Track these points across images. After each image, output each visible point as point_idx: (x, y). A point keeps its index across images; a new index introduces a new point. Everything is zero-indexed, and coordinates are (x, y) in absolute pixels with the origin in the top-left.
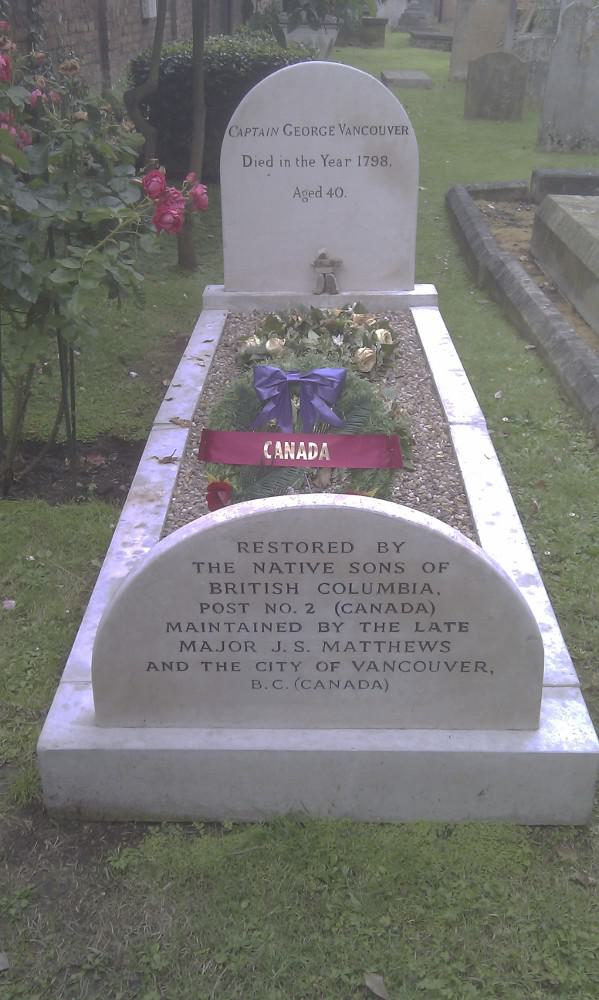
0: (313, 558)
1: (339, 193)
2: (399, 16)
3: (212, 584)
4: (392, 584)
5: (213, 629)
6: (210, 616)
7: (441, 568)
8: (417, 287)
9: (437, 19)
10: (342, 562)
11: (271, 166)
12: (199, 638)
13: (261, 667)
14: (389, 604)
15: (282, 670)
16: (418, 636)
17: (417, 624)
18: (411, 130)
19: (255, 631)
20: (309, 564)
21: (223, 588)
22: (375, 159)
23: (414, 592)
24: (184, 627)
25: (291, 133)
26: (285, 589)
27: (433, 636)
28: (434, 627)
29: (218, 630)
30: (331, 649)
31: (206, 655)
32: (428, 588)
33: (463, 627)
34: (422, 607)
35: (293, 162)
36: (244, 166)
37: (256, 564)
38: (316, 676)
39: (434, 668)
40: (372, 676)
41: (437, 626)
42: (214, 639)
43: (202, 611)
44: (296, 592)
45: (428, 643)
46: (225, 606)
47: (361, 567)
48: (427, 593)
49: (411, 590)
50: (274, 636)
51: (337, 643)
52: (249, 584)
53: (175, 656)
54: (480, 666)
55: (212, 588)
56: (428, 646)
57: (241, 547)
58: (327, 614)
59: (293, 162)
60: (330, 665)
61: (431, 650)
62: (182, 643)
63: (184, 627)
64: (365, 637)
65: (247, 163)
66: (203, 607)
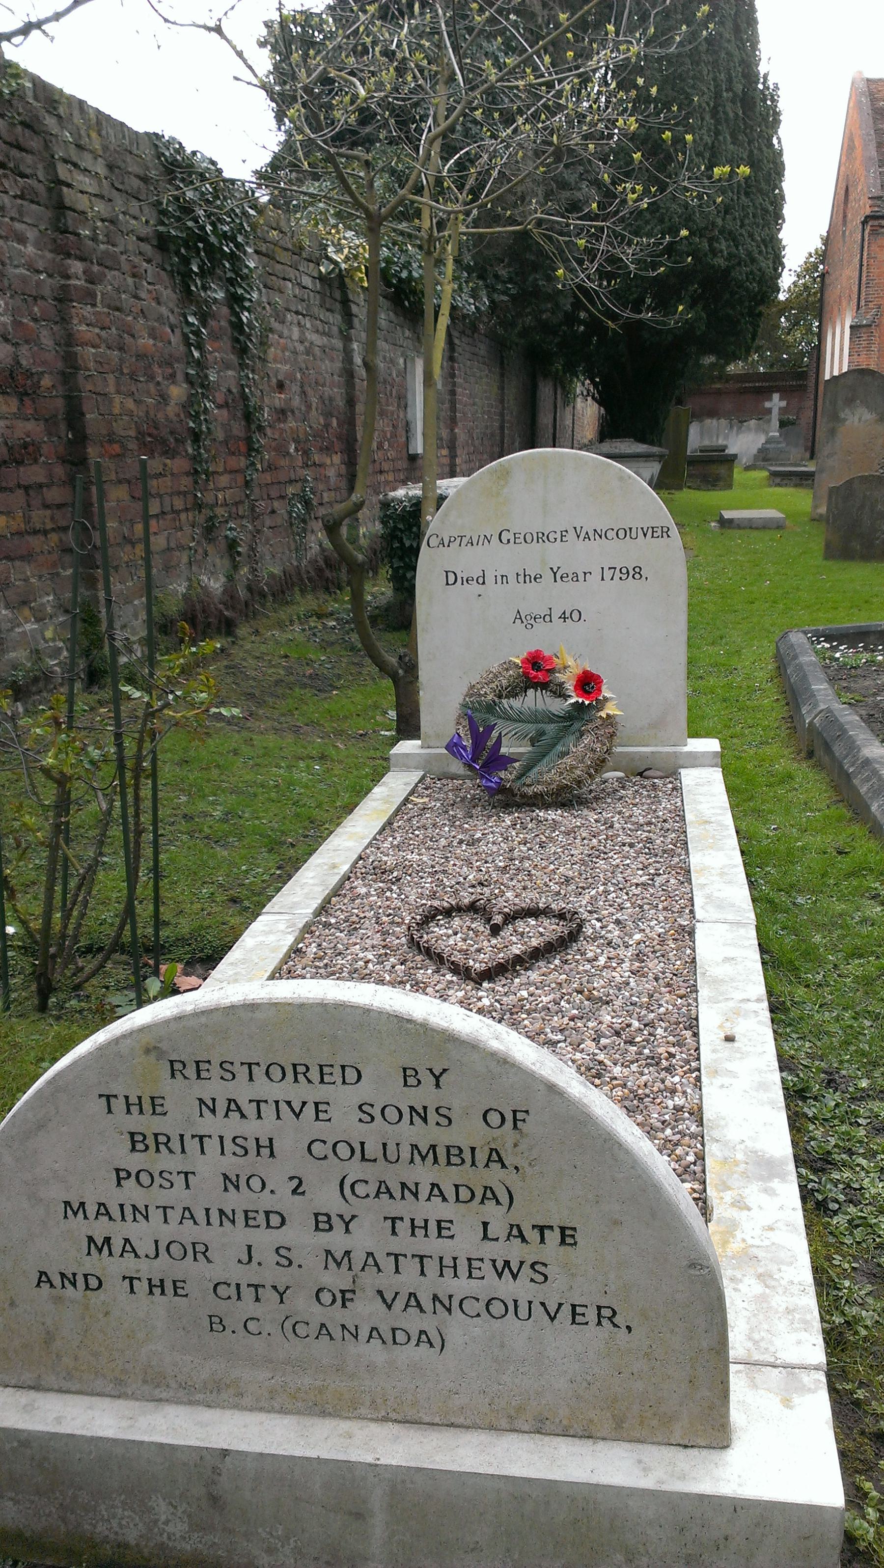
0: (297, 1092)
1: (575, 616)
2: (755, 451)
3: (132, 1135)
4: (433, 1147)
6: (131, 1192)
7: (515, 1120)
8: (690, 741)
9: (808, 455)
10: (343, 1099)
11: (484, 583)
12: (118, 1231)
13: (221, 1289)
15: (257, 1299)
16: (489, 1250)
17: (485, 1225)
18: (674, 531)
19: (209, 1223)
20: (289, 1103)
21: (150, 1141)
23: (473, 1164)
24: (91, 1209)
25: (509, 541)
26: (253, 1151)
27: (515, 1251)
28: (515, 1232)
29: (146, 1218)
30: (339, 1264)
31: (129, 1264)
32: (496, 1157)
33: (567, 1235)
34: (489, 1194)
35: (512, 578)
36: (447, 584)
37: (201, 1100)
38: (316, 1313)
39: (523, 1312)
40: (413, 1322)
41: (520, 1231)
42: (142, 1233)
43: (119, 1184)
44: (272, 1154)
45: (507, 1263)
48: (496, 1166)
49: (468, 1160)
50: (240, 1235)
51: (347, 1253)
52: (193, 1136)
55: (133, 1143)
56: (505, 1268)
59: (512, 578)
60: (339, 1296)
61: (515, 1276)
62: (91, 1239)
63: (91, 1209)
65: (451, 581)
66: (121, 1176)
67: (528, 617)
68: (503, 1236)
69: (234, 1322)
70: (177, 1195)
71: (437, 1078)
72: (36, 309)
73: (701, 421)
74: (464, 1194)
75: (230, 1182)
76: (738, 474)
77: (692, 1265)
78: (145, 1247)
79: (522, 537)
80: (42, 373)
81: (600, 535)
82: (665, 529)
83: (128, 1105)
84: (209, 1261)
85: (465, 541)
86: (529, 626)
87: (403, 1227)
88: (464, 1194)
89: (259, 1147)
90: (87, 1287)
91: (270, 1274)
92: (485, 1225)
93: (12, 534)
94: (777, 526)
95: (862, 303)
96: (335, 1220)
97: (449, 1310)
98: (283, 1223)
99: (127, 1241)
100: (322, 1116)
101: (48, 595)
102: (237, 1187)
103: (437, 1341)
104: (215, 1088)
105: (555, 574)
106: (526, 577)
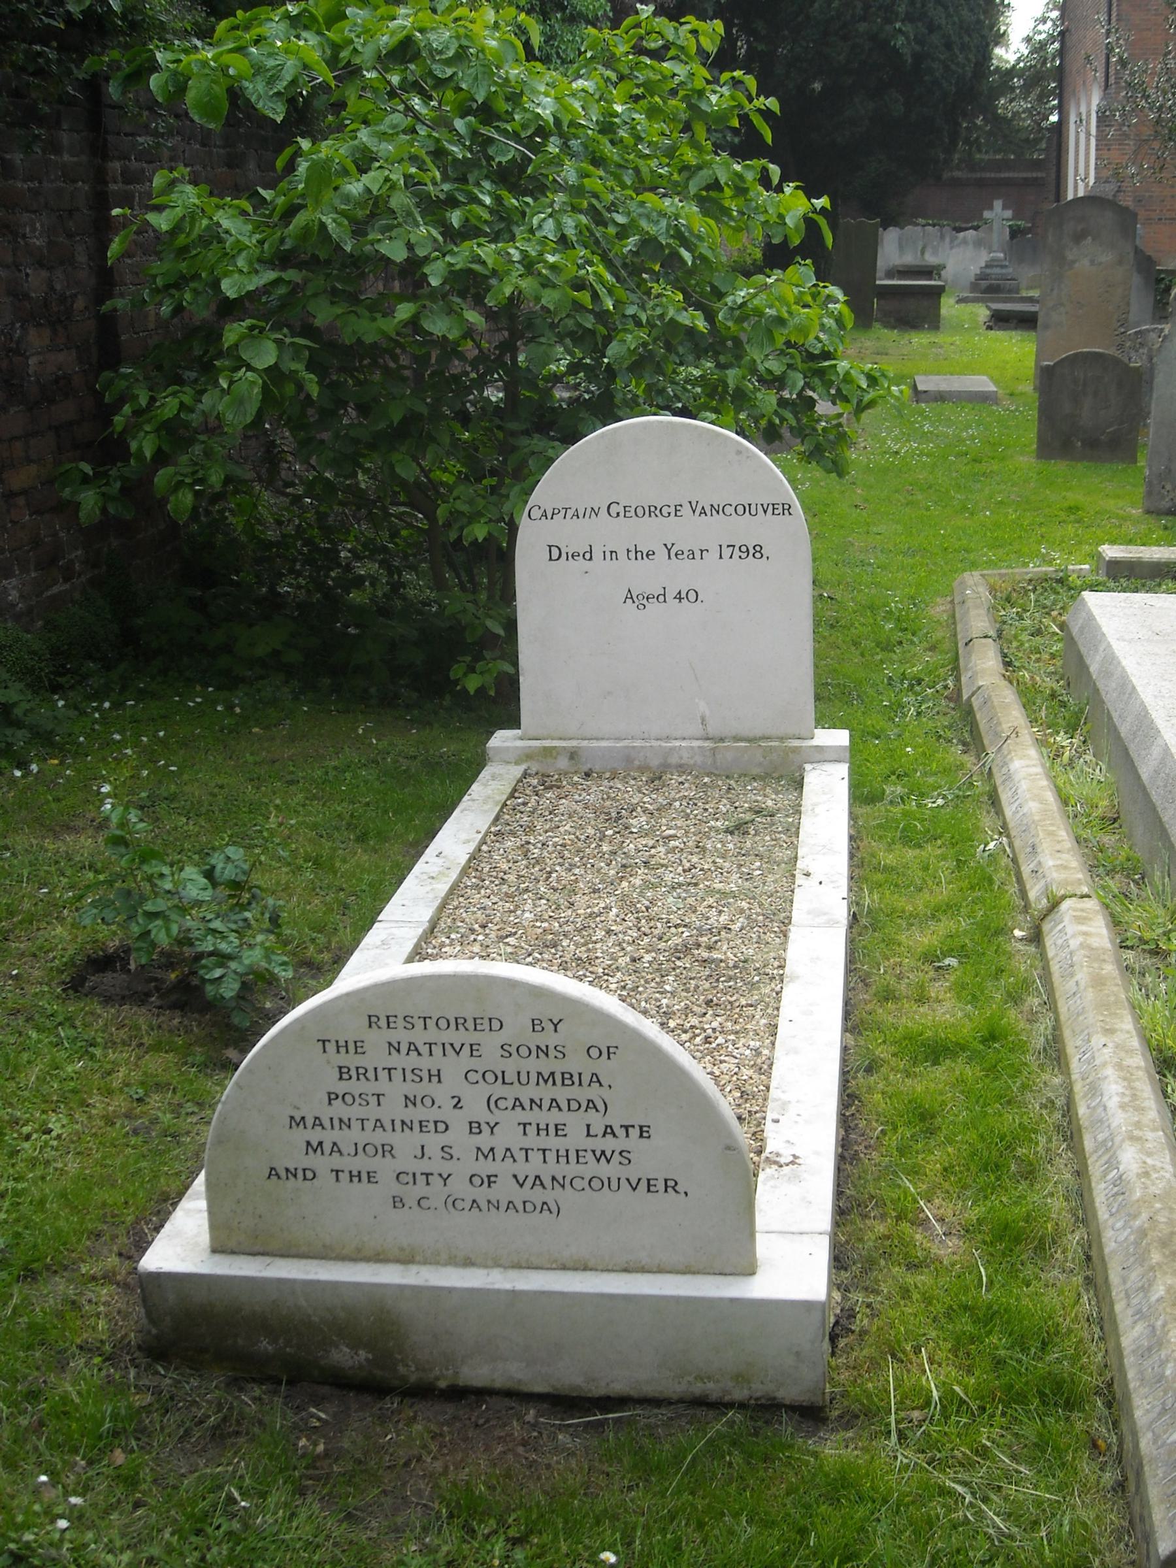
1: (692, 596)
3: (340, 1068)
4: (552, 1074)
5: (343, 1126)
8: (819, 732)
10: (491, 1042)
11: (591, 559)
14: (552, 1100)
15: (428, 1184)
16: (590, 1143)
20: (452, 1045)
21: (353, 1073)
22: (743, 549)
23: (580, 1084)
25: (618, 514)
26: (426, 1078)
27: (609, 1144)
30: (486, 1157)
31: (336, 1161)
32: (596, 1079)
33: (643, 1132)
35: (622, 555)
36: (551, 559)
38: (470, 1193)
40: (538, 1196)
42: (347, 1138)
43: (330, 1104)
44: (439, 1081)
45: (603, 1152)
46: (357, 1097)
47: (513, 1050)
49: (577, 1082)
51: (492, 1149)
53: (301, 1160)
54: (671, 1185)
55: (341, 1073)
57: (372, 1021)
58: (476, 1109)
59: (622, 555)
60: (486, 1180)
62: (308, 1143)
63: (310, 1121)
64: (528, 1142)
67: (640, 597)
68: (601, 1133)
69: (411, 1202)
70: (372, 1112)
71: (556, 1026)
72: (71, 223)
73: (902, 228)
74: (574, 1106)
75: (410, 1101)
76: (948, 307)
77: (728, 1148)
78: (348, 1149)
79: (633, 510)
80: (75, 295)
81: (717, 510)
82: (786, 507)
83: (338, 1047)
84: (393, 1157)
85: (570, 513)
86: (641, 607)
87: (532, 1130)
88: (574, 1106)
89: (430, 1076)
90: (305, 1179)
91: (436, 1165)
92: (588, 1126)
93: (43, 484)
94: (983, 398)
95: (1112, 80)
96: (484, 1127)
97: (563, 1186)
98: (447, 1129)
99: (335, 1144)
100: (475, 1053)
101: (77, 549)
102: (415, 1104)
103: (554, 1209)
104: (400, 1035)
105: (669, 551)
106: (637, 554)
